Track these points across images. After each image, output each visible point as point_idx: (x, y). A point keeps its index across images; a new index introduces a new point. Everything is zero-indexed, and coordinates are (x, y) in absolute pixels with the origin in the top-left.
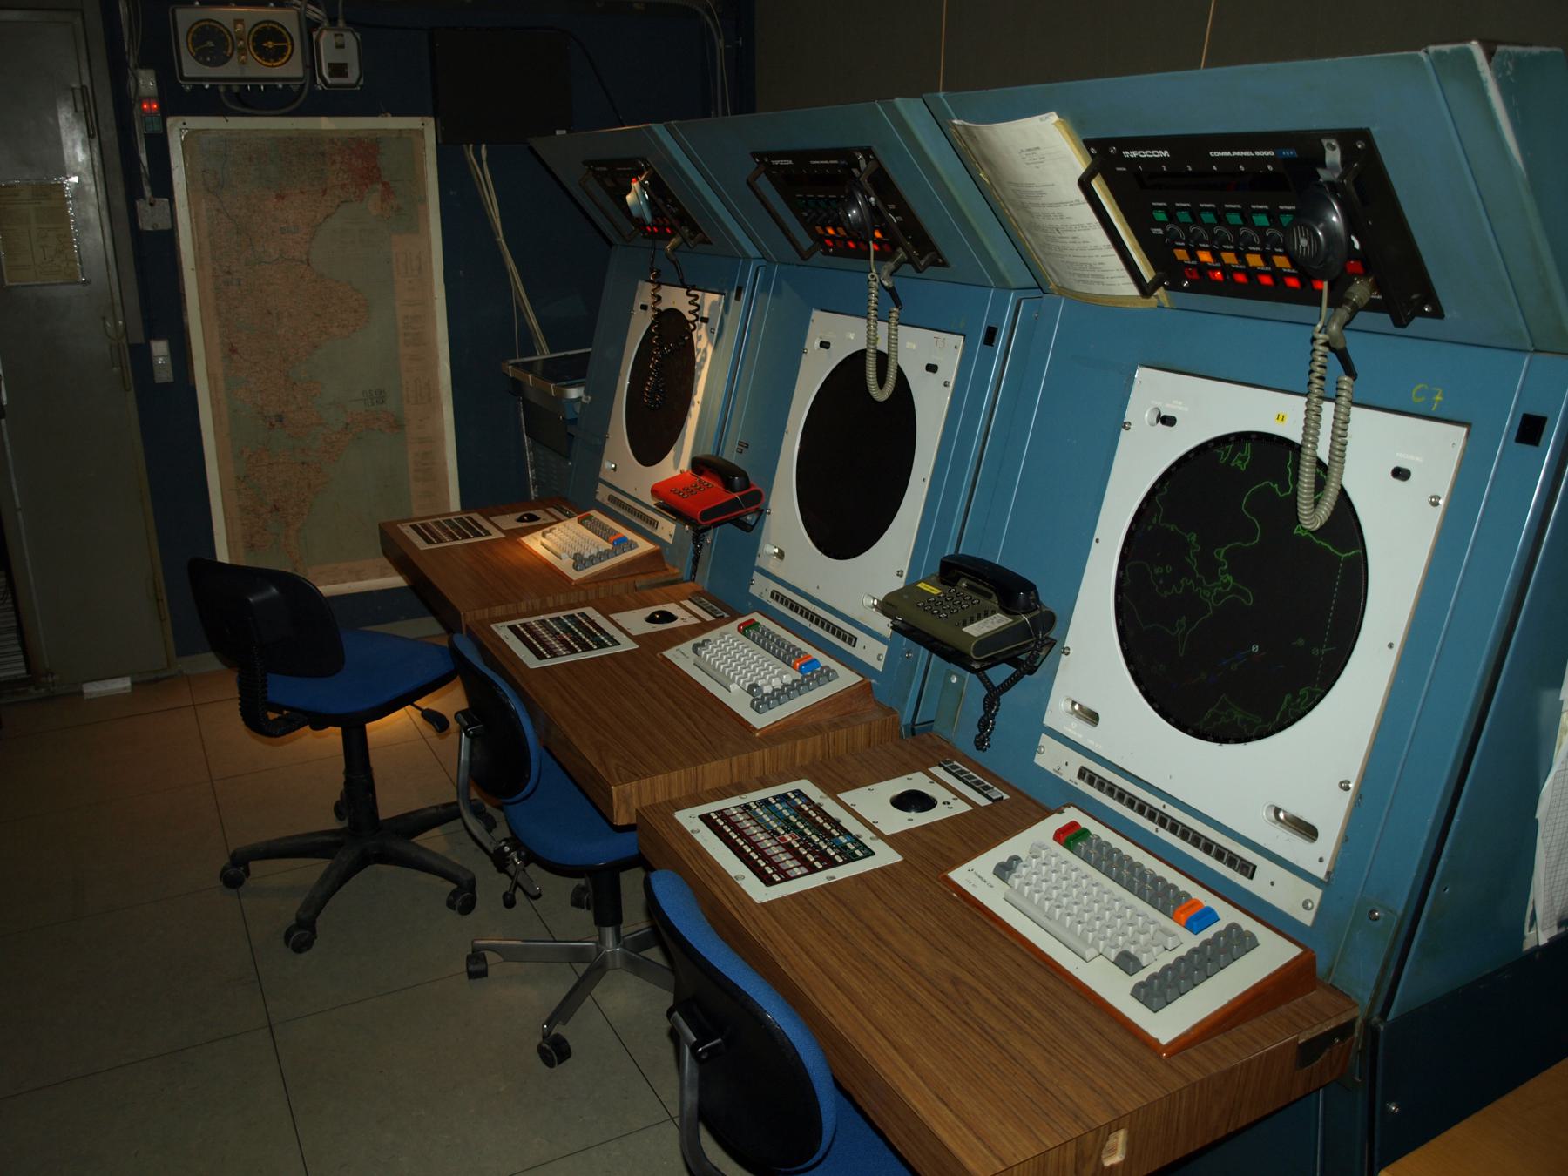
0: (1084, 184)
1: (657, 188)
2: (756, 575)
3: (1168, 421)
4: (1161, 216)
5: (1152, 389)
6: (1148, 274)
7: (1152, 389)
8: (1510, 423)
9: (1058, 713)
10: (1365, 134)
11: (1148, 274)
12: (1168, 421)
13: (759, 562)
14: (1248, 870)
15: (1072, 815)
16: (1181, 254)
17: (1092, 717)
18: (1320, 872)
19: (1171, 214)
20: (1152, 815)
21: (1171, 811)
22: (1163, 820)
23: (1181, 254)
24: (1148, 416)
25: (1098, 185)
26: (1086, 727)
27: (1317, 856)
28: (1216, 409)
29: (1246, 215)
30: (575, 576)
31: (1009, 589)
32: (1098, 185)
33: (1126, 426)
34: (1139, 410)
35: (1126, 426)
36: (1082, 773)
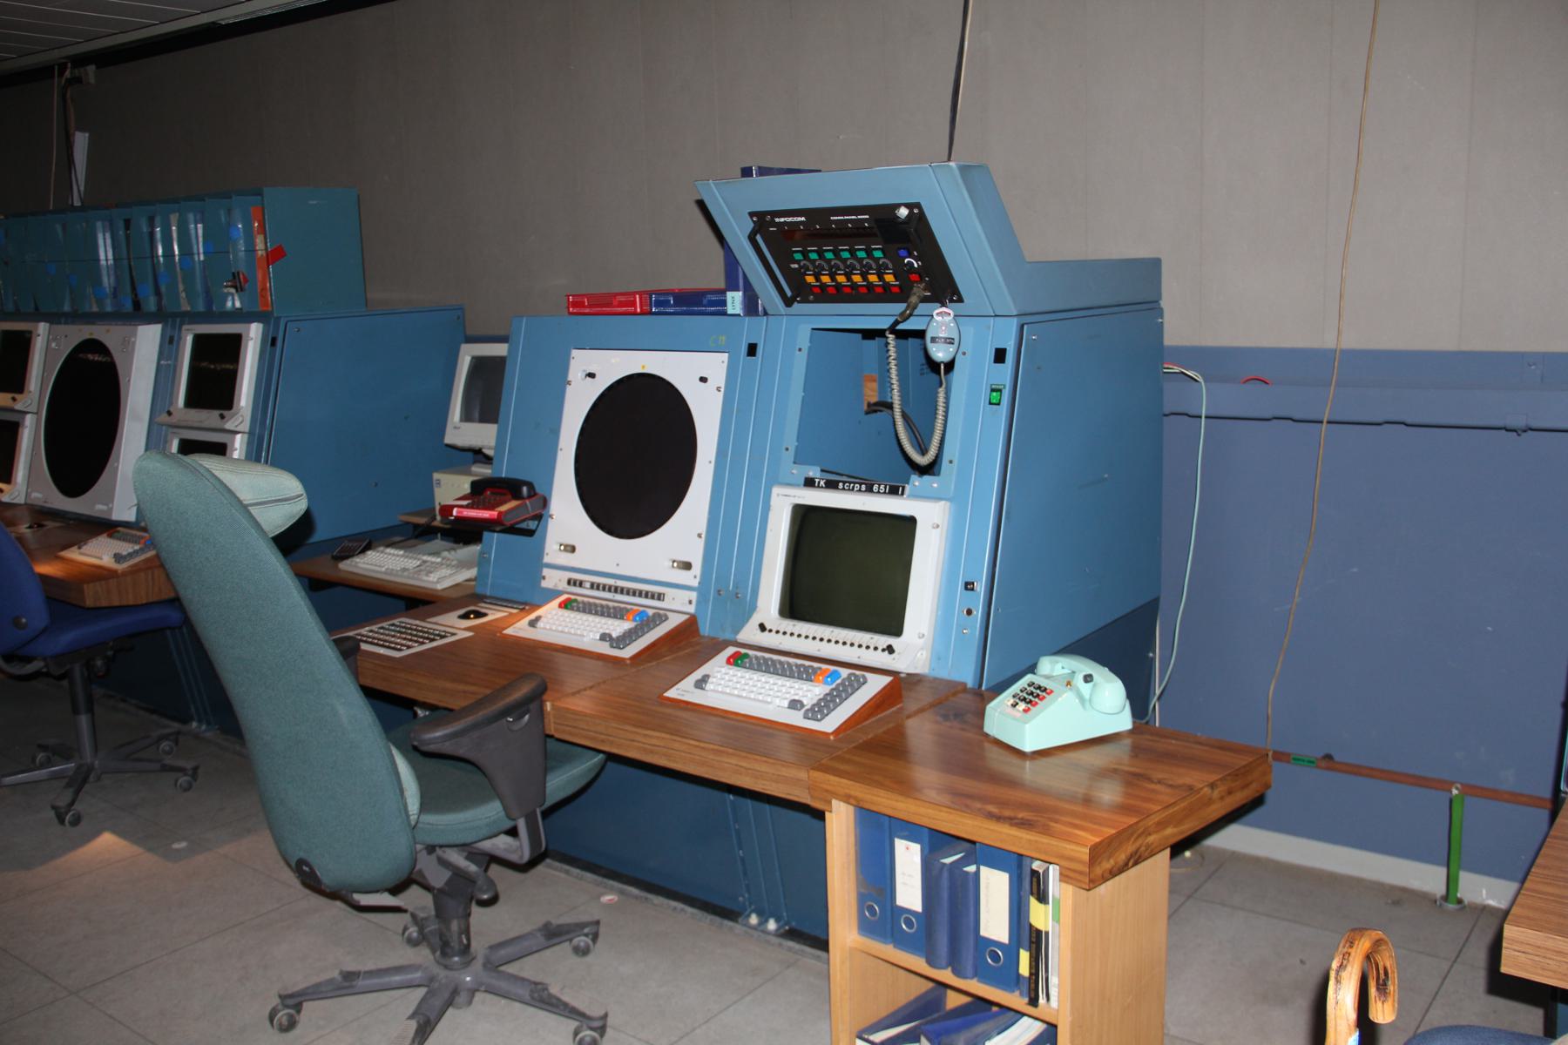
0: (752, 239)
1: (907, 205)
2: (546, 572)
3: (591, 375)
4: (798, 256)
5: (581, 361)
6: (789, 293)
7: (581, 361)
8: (744, 349)
9: (552, 553)
10: (918, 205)
11: (789, 293)
12: (591, 375)
13: (547, 559)
14: (660, 597)
15: (731, 650)
16: (810, 279)
17: (573, 549)
18: (695, 583)
19: (805, 254)
20: (610, 589)
21: (620, 583)
22: (616, 590)
23: (810, 279)
24: (581, 375)
25: (758, 238)
26: (684, 573)
27: (691, 578)
28: (615, 365)
29: (869, 252)
30: (120, 567)
31: (511, 488)
32: (758, 238)
33: (569, 383)
34: (576, 370)
35: (569, 383)
36: (569, 582)
